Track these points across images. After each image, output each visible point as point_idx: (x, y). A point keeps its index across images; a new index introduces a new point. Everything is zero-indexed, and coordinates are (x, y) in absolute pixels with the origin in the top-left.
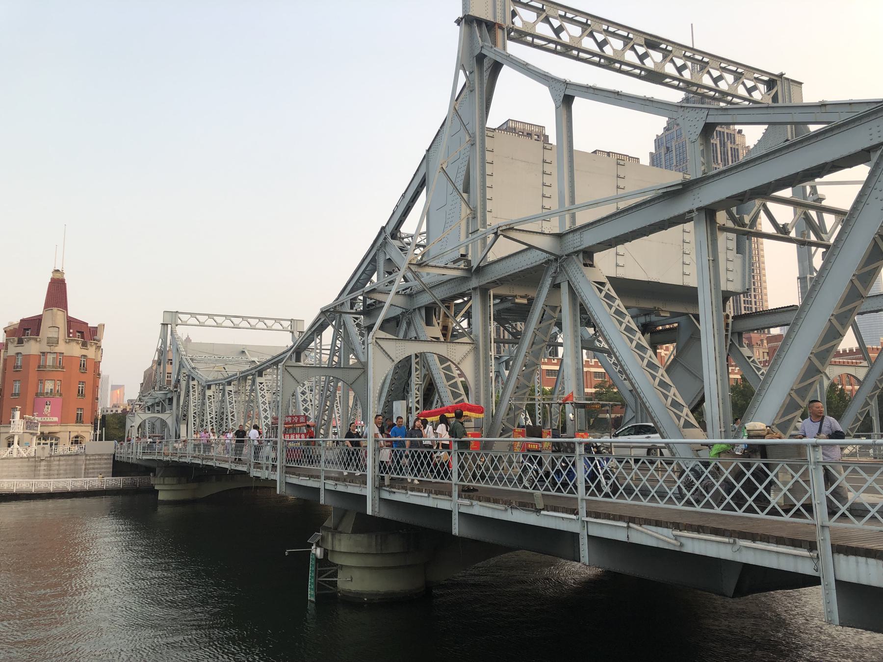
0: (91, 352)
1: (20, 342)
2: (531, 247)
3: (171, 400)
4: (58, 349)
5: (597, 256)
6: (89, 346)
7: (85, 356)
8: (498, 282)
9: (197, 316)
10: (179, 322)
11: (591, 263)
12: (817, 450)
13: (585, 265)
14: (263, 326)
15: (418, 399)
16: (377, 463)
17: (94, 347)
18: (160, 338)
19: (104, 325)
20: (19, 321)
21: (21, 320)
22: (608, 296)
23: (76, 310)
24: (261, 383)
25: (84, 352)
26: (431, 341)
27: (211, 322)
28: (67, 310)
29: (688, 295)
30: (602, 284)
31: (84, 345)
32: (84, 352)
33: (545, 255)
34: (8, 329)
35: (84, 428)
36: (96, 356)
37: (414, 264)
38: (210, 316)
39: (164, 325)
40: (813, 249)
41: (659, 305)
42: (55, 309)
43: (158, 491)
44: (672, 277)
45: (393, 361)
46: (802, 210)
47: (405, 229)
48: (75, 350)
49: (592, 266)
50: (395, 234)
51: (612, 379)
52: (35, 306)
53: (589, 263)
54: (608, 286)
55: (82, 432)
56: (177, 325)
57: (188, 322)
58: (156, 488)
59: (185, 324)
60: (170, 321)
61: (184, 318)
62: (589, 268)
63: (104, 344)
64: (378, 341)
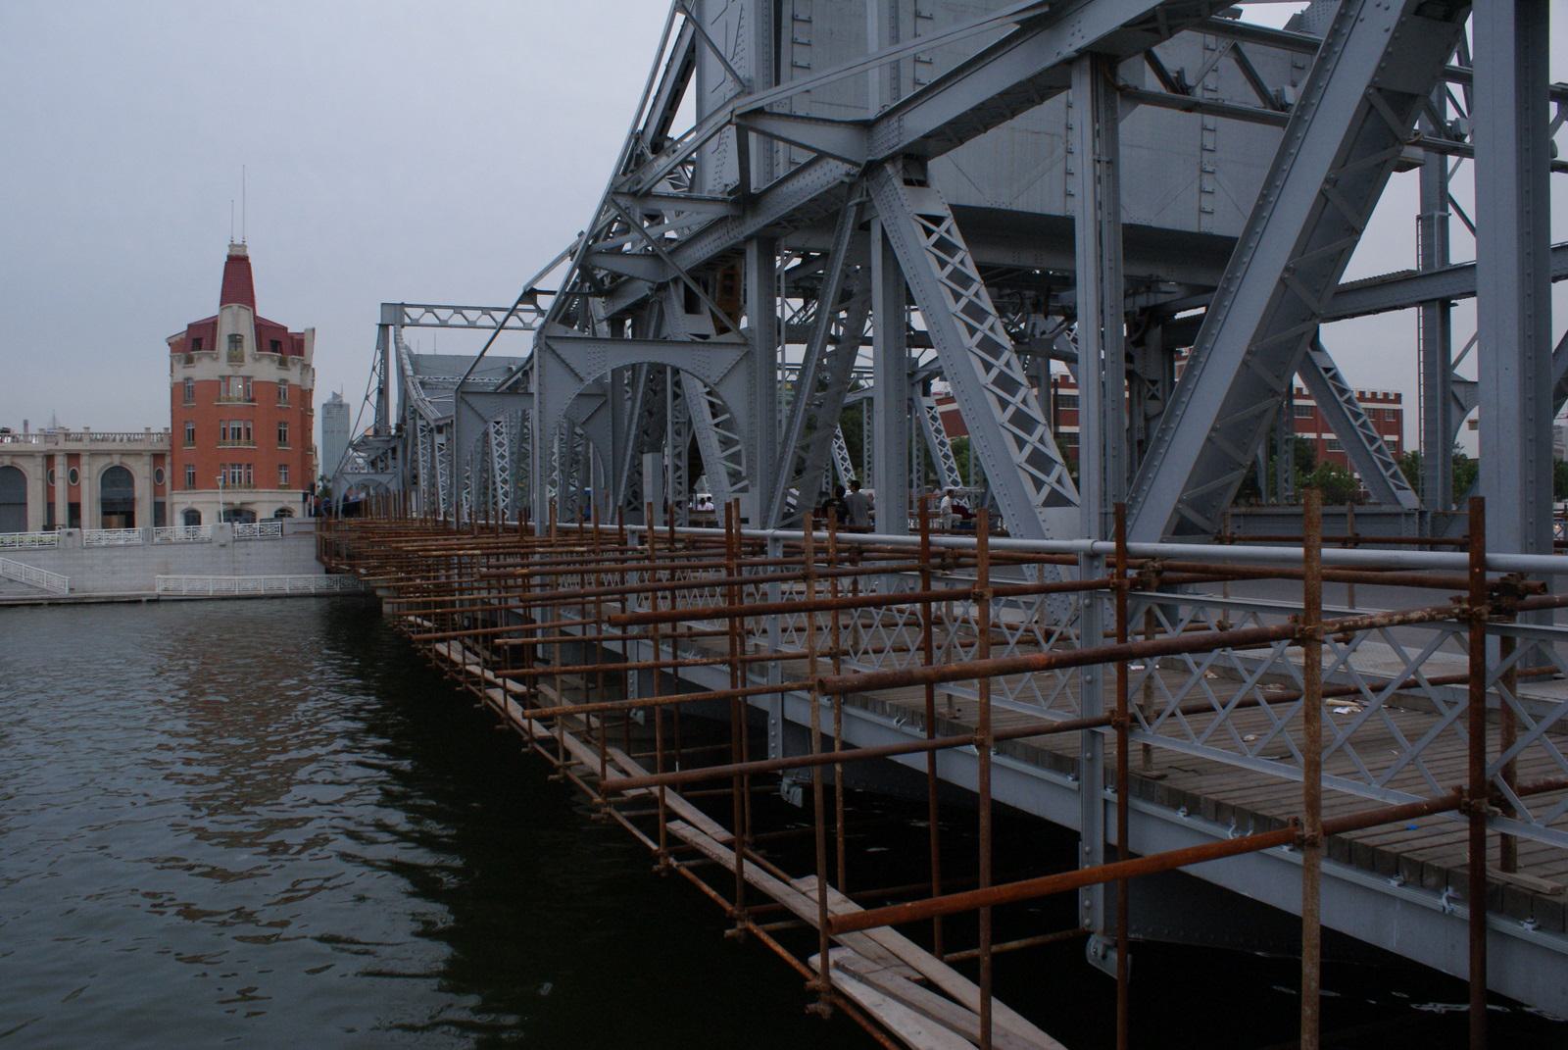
0: (293, 376)
1: (189, 360)
2: (821, 156)
3: (394, 450)
4: (245, 371)
5: (933, 165)
6: (289, 365)
7: (284, 381)
8: (785, 224)
9: (464, 312)
10: (407, 320)
11: (921, 178)
12: (1096, 563)
13: (908, 182)
14: (461, 321)
15: (678, 450)
16: (1111, 509)
17: (299, 367)
18: (377, 348)
19: (314, 330)
20: (185, 328)
21: (190, 326)
22: (943, 245)
23: (271, 305)
24: (498, 423)
25: (284, 374)
26: (693, 342)
27: (458, 319)
28: (253, 306)
29: (1057, 232)
30: (937, 220)
31: (283, 363)
32: (284, 374)
33: (846, 167)
34: (173, 341)
35: (291, 498)
36: (302, 380)
37: (623, 194)
38: (458, 309)
39: (384, 327)
40: (1452, 160)
41: (1160, 271)
42: (235, 306)
43: (381, 598)
44: (1041, 200)
45: (581, 380)
46: (1228, 41)
47: (675, 131)
48: (266, 370)
49: (923, 183)
50: (660, 142)
51: (102, 440)
52: (206, 302)
53: (918, 180)
54: (949, 222)
55: (290, 502)
56: (403, 326)
57: (421, 321)
58: (379, 593)
59: (415, 323)
60: (394, 316)
61: (414, 313)
62: (917, 189)
63: (316, 363)
64: (549, 343)
